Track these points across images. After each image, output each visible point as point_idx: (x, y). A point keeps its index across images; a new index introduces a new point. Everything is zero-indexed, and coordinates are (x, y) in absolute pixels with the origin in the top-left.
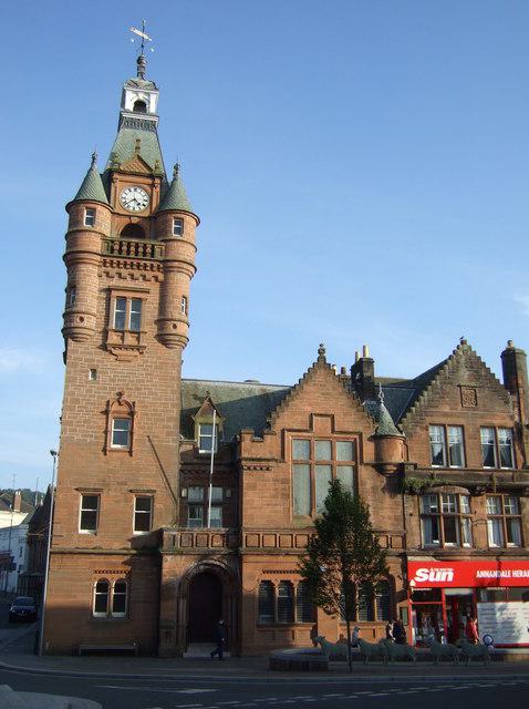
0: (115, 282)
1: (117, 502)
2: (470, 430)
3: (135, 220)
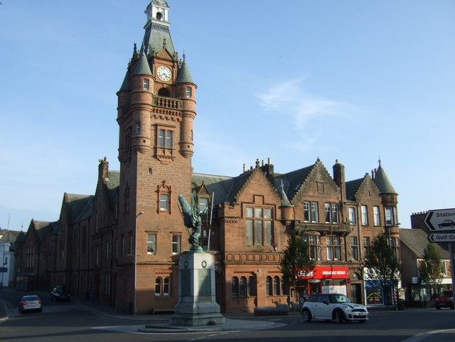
0: (158, 121)
2: (320, 203)
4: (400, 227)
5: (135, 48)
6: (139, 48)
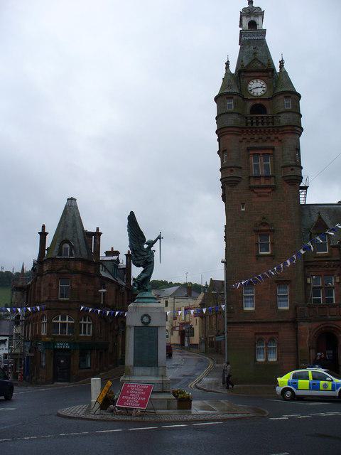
0: (252, 144)
1: (266, 289)
3: (258, 102)
4: (220, 276)
5: (227, 64)
6: (233, 69)
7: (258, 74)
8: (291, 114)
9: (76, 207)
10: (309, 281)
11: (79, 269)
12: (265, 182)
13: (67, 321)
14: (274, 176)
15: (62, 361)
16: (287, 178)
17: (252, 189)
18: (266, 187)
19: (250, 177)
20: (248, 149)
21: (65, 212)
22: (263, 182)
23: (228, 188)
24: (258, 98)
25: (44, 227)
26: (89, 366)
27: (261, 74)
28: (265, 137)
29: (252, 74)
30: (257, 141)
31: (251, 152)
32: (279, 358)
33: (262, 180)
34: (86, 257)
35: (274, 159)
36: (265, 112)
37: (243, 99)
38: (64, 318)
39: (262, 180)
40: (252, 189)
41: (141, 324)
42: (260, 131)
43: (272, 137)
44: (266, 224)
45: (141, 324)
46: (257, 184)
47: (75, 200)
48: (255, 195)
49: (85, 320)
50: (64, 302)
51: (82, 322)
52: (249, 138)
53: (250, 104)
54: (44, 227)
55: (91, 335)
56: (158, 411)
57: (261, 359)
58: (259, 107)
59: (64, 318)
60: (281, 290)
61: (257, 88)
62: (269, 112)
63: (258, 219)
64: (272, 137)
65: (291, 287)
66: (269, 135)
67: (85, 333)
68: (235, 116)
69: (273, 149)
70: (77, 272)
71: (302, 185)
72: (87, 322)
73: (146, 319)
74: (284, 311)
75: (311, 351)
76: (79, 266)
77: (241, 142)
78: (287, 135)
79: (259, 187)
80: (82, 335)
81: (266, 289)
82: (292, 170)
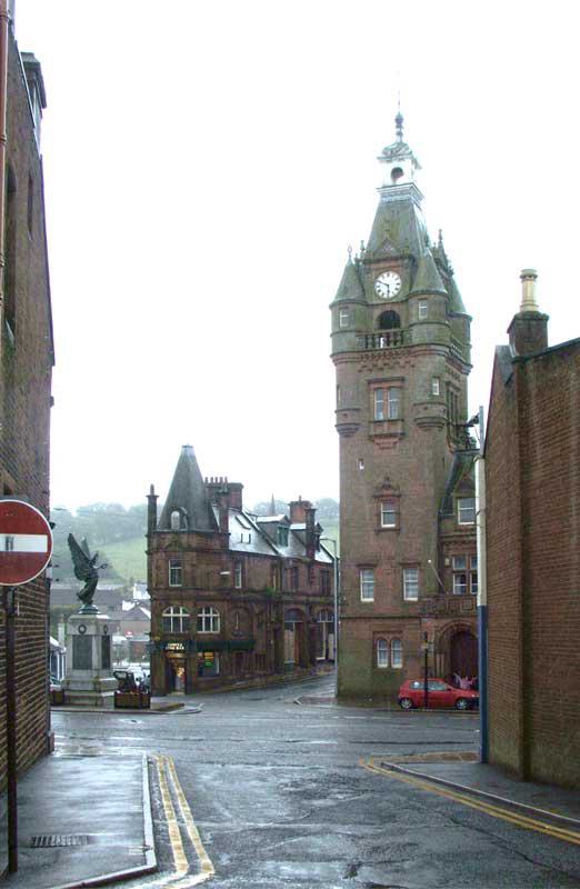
0: (373, 376)
3: (388, 308)
5: (362, 242)
7: (388, 264)
8: (425, 326)
9: (193, 458)
10: (447, 561)
11: (194, 545)
12: (389, 428)
13: (181, 614)
14: (403, 420)
15: (416, 684)
16: (419, 421)
17: (371, 438)
18: (391, 436)
19: (370, 422)
20: (369, 382)
21: (180, 467)
22: (385, 429)
23: (345, 439)
24: (388, 302)
25: (152, 488)
26: (218, 671)
27: (393, 264)
28: (391, 363)
29: (382, 265)
30: (382, 369)
31: (373, 386)
32: (404, 664)
33: (386, 424)
34: (205, 529)
35: (403, 393)
36: (397, 324)
37: (368, 305)
38: (177, 611)
39: (386, 424)
40: (371, 438)
41: (78, 633)
42: (391, 354)
43: (402, 362)
44: (390, 486)
45: (78, 633)
46: (379, 431)
47: (191, 447)
48: (377, 447)
49: (208, 612)
50: (176, 589)
51: (203, 615)
52: (371, 366)
53: (377, 313)
54: (152, 488)
55: (218, 632)
56: (104, 695)
57: (383, 665)
58: (389, 320)
59: (177, 611)
60: (410, 575)
61: (389, 285)
62: (403, 324)
63: (381, 480)
64: (402, 362)
65: (421, 570)
66: (387, 361)
67: (208, 628)
68: (353, 334)
69: (403, 379)
70: (189, 549)
71: (470, 416)
72: (211, 615)
73: (82, 629)
74: (413, 603)
75: (438, 656)
76: (194, 541)
77: (360, 371)
78: (420, 358)
79: (380, 436)
80: (204, 631)
81: (388, 574)
82: (426, 408)
